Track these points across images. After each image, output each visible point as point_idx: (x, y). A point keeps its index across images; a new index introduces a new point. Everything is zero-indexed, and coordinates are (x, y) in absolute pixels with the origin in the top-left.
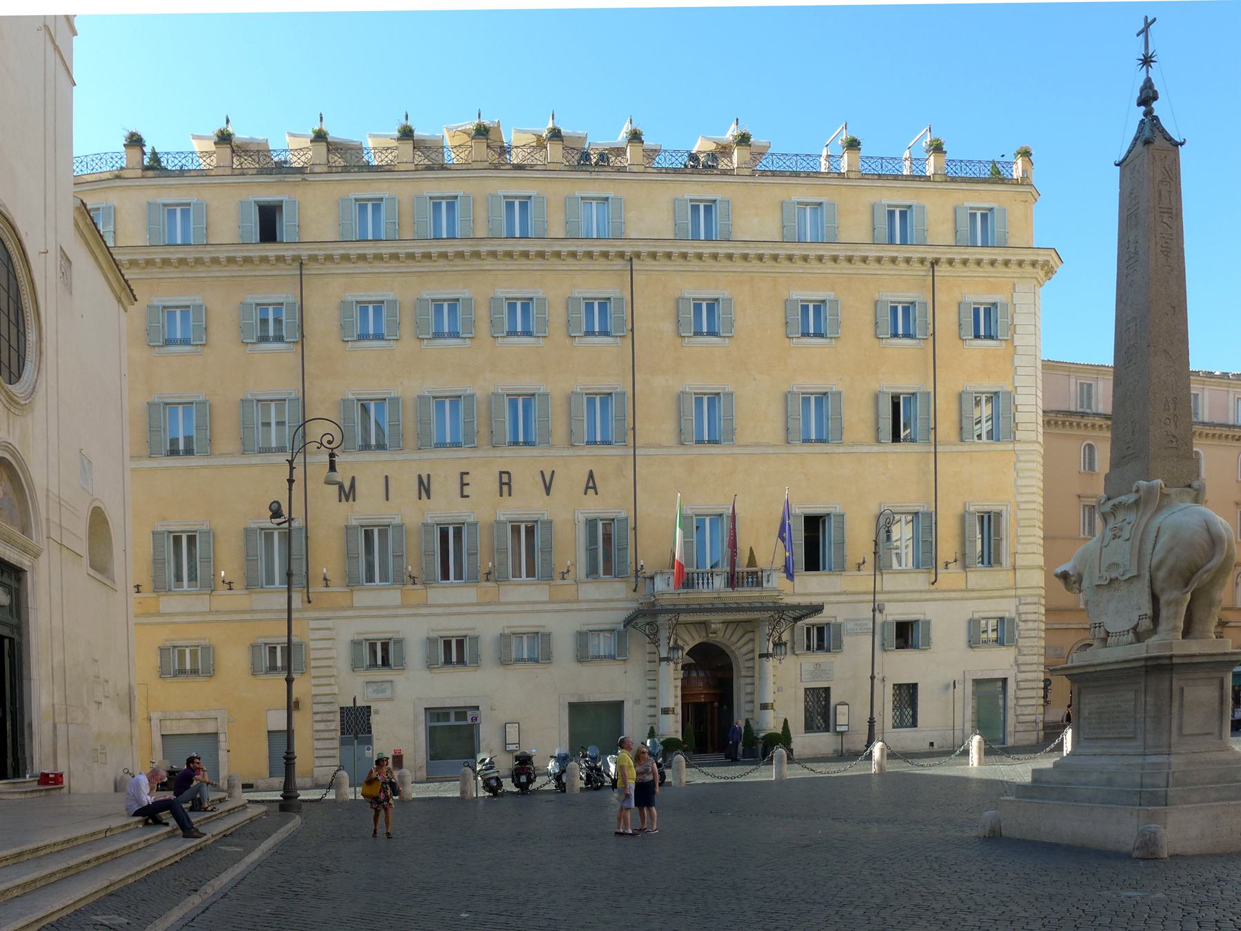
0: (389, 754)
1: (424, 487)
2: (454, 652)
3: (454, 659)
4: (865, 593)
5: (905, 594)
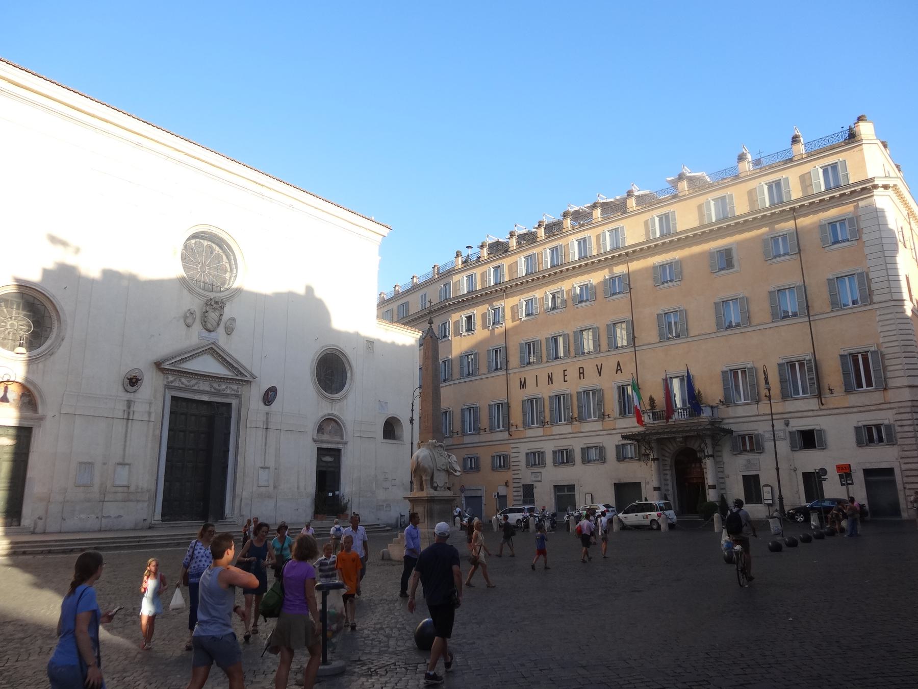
2: (564, 457)
4: (764, 415)
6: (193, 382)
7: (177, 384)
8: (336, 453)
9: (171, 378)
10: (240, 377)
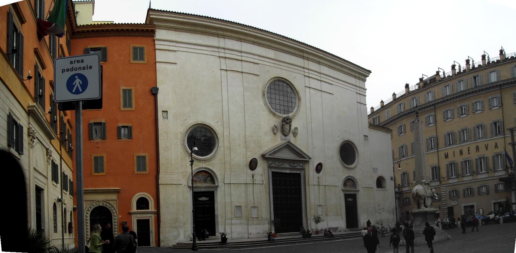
1: (461, 153)
6: (281, 164)
7: (273, 165)
8: (354, 197)
9: (270, 163)
10: (302, 159)
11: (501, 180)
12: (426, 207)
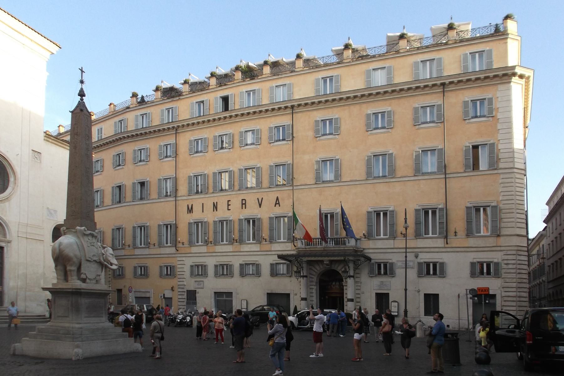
0: (155, 307)
1: (215, 207)
2: (224, 270)
3: (431, 273)
5: (430, 248)
11: (280, 257)
12: (84, 281)
